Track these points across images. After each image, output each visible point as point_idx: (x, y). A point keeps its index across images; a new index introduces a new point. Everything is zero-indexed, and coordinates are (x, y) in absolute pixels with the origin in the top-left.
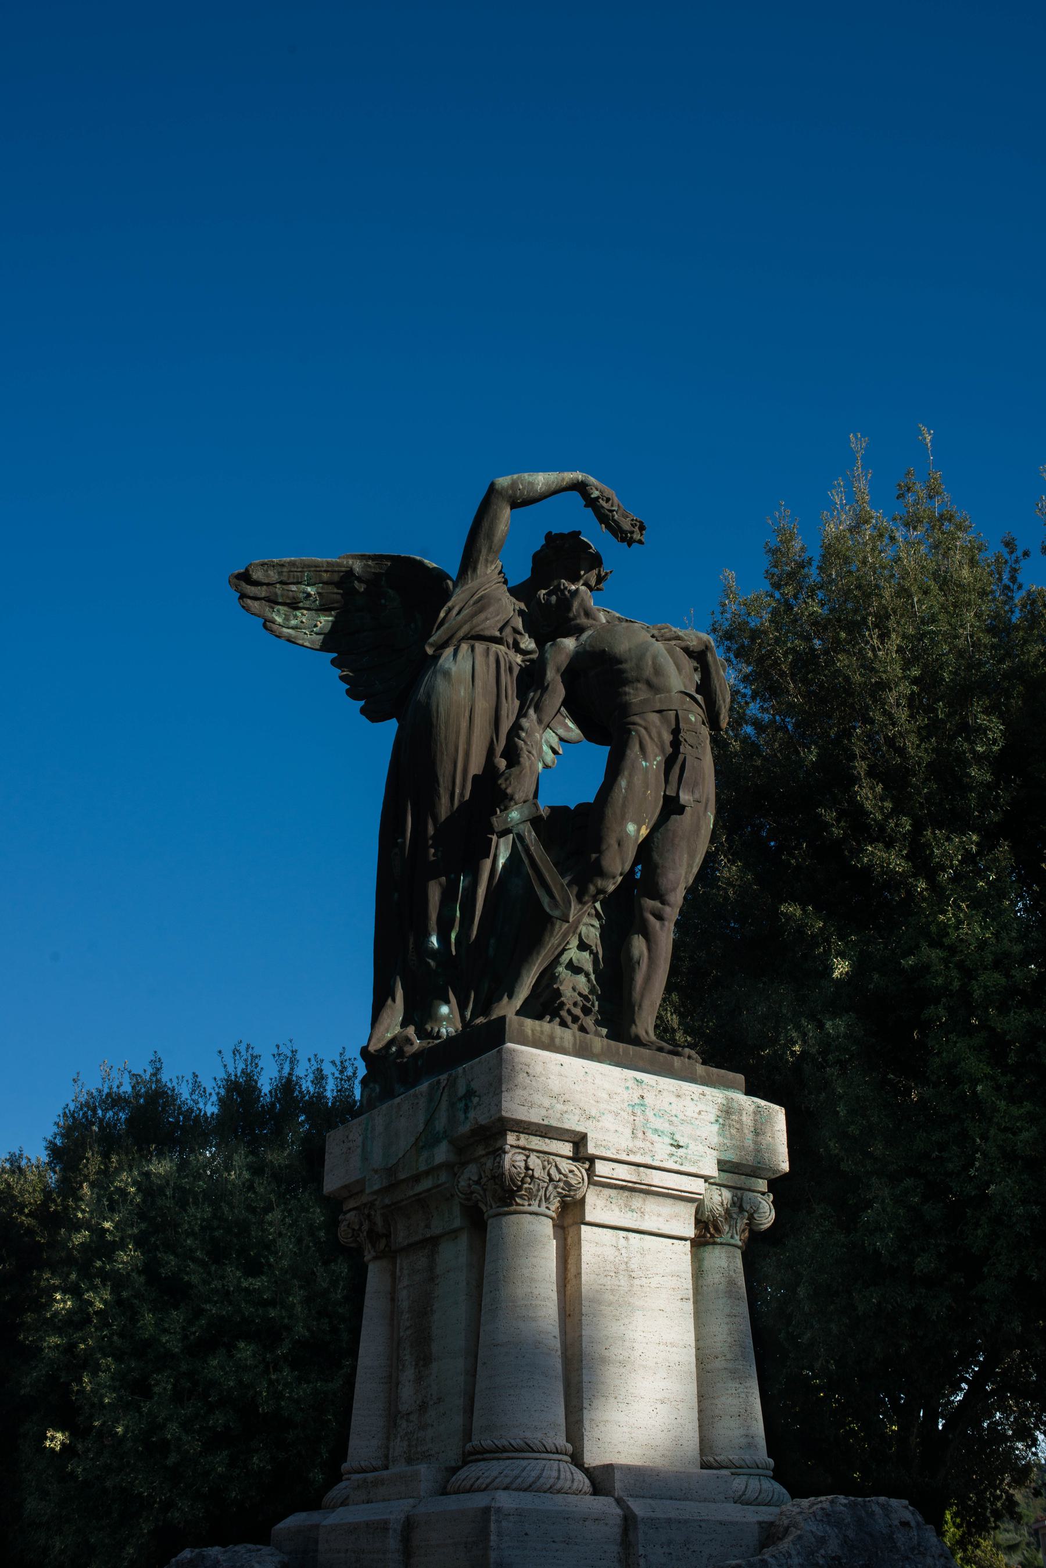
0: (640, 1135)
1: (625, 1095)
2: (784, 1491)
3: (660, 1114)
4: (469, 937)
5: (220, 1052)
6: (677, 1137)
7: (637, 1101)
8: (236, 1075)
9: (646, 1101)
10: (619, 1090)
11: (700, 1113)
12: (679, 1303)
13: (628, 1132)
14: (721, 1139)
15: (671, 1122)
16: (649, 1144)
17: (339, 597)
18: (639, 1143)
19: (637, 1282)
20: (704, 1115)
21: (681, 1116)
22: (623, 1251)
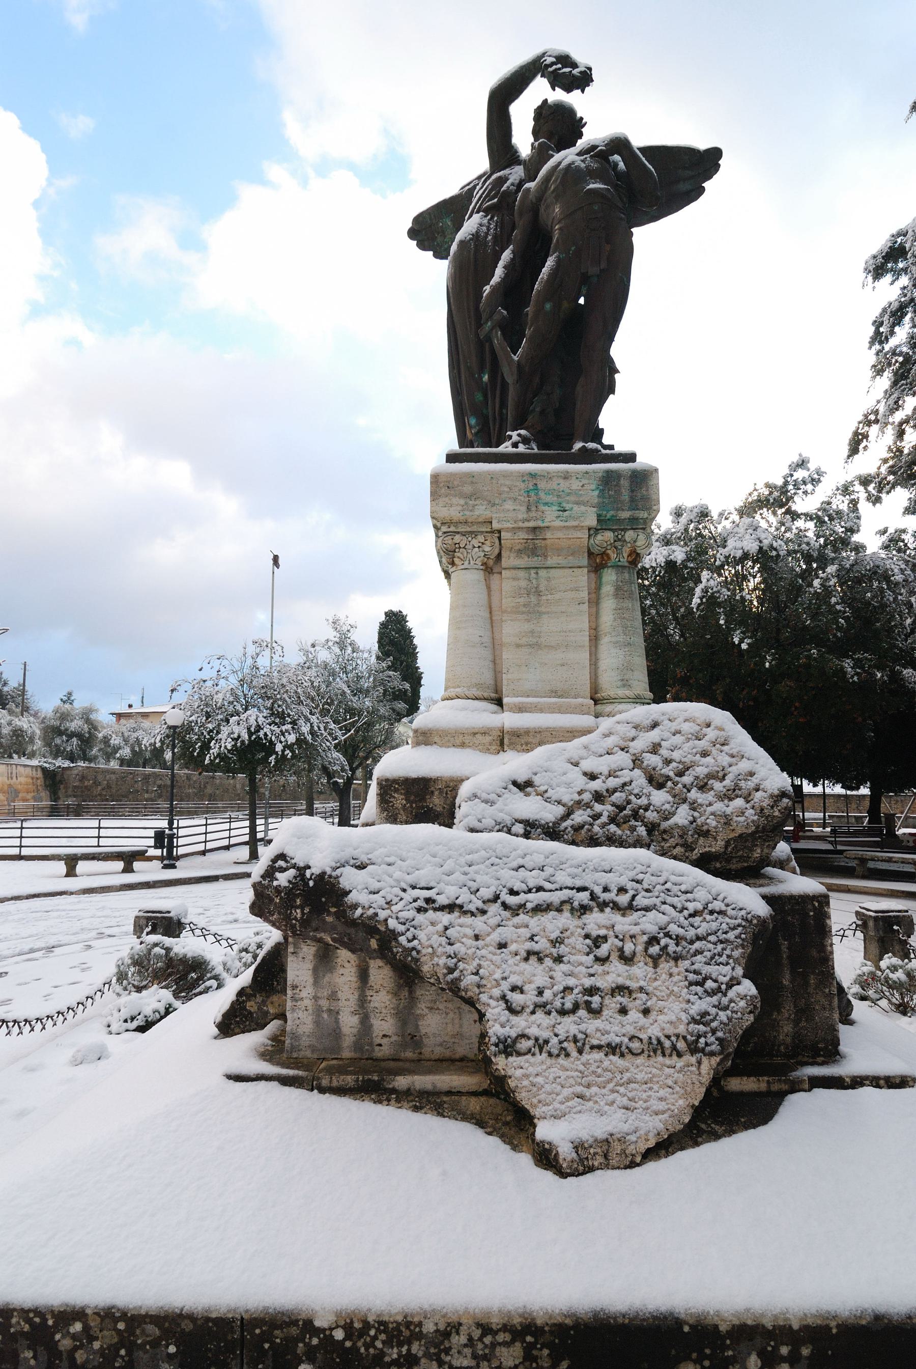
0: (534, 509)
1: (522, 485)
2: (700, 710)
3: (549, 492)
4: (559, 262)
5: (201, 670)
6: (564, 505)
7: (532, 487)
8: (431, 219)
9: (539, 486)
10: (518, 484)
11: (583, 486)
12: (577, 606)
13: (524, 509)
14: (601, 500)
15: (559, 496)
16: (540, 513)
17: (182, 832)
18: (533, 514)
19: (544, 598)
20: (586, 487)
21: (567, 491)
22: (534, 581)
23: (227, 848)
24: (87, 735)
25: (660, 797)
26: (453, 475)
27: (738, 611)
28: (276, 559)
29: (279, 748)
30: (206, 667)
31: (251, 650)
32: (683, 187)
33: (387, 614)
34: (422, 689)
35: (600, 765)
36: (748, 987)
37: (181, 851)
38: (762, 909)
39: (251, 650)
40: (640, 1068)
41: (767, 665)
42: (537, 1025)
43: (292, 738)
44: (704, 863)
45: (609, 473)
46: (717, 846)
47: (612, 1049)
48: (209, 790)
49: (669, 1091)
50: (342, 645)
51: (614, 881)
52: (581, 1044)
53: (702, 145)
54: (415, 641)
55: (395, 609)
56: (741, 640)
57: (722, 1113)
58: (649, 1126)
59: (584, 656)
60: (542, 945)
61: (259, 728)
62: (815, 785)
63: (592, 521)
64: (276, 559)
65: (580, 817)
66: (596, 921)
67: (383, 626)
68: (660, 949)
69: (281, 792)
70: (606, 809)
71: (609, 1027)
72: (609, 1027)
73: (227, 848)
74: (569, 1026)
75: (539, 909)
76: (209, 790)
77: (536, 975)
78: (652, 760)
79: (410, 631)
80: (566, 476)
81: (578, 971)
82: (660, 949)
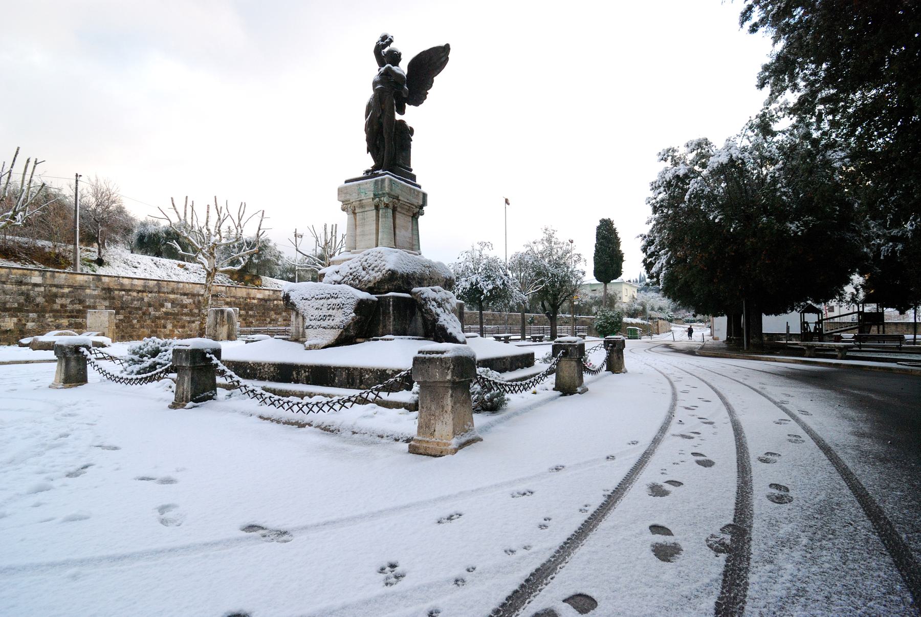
24: (501, 287)
25: (364, 273)
26: (350, 186)
27: (711, 198)
28: (507, 201)
29: (485, 292)
31: (478, 247)
32: (443, 59)
34: (623, 264)
35: (352, 266)
36: (354, 315)
39: (478, 247)
40: (327, 331)
42: (312, 323)
43: (490, 287)
46: (371, 285)
48: (510, 322)
51: (335, 292)
53: (443, 44)
54: (619, 236)
55: (606, 218)
56: (715, 217)
58: (325, 342)
59: (374, 237)
61: (477, 283)
62: (902, 312)
63: (372, 196)
64: (507, 201)
65: (346, 279)
66: (329, 301)
67: (599, 228)
68: (340, 307)
70: (351, 277)
71: (324, 324)
72: (324, 324)
74: (319, 323)
76: (510, 322)
77: (317, 313)
78: (365, 263)
79: (615, 230)
81: (325, 312)
82: (340, 307)
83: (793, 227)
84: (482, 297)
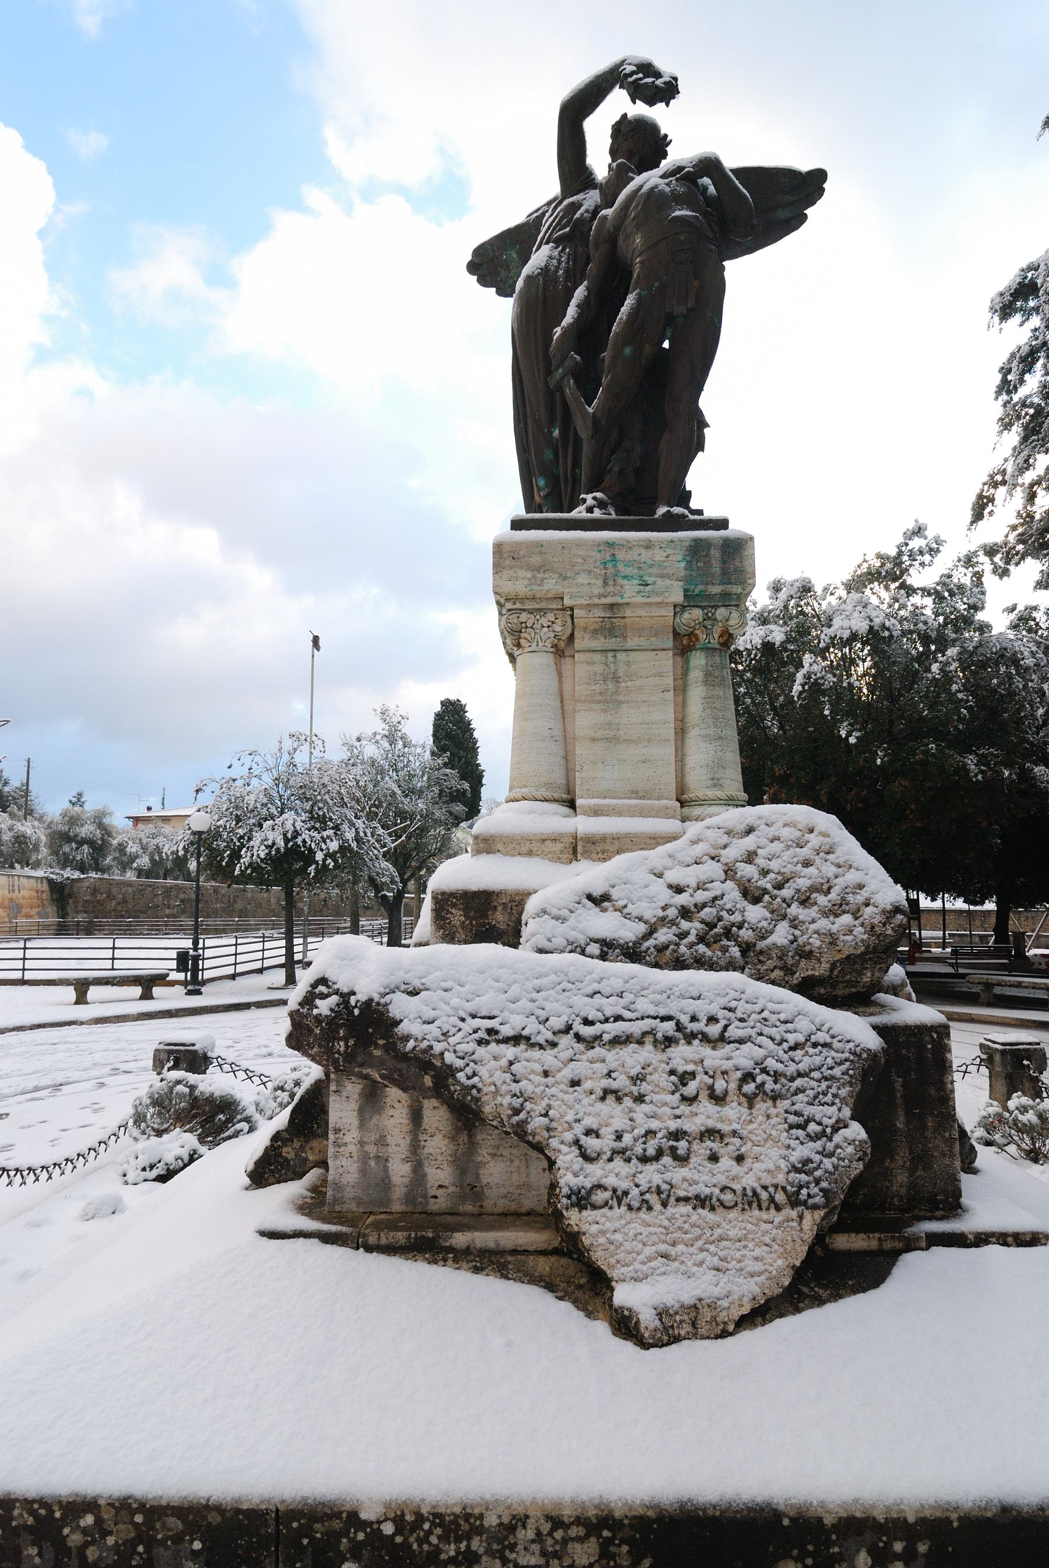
23: (260, 971)
24: (100, 842)
25: (755, 913)
26: (518, 544)
27: (845, 699)
28: (316, 641)
29: (319, 856)
30: (236, 764)
31: (288, 744)
32: (782, 214)
33: (443, 703)
35: (688, 876)
36: (856, 1131)
37: (207, 974)
38: (873, 1041)
39: (288, 744)
40: (733, 1223)
41: (879, 761)
42: (615, 1174)
43: (334, 846)
44: (807, 988)
45: (697, 541)
46: (821, 969)
47: (701, 1202)
48: (239, 905)
49: (766, 1249)
50: (391, 738)
51: (703, 1009)
52: (665, 1196)
53: (804, 166)
54: (476, 735)
55: (453, 698)
57: (827, 1274)
58: (744, 1290)
59: (670, 751)
60: (621, 1082)
61: (296, 834)
62: (933, 900)
63: (678, 597)
64: (316, 641)
65: (664, 935)
66: (682, 1055)
67: (439, 717)
68: (755, 1087)
69: (322, 907)
70: (694, 927)
71: (698, 1176)
72: (698, 1176)
73: (260, 971)
74: (651, 1175)
75: (618, 1041)
76: (239, 905)
77: (614, 1116)
78: (747, 871)
79: (469, 723)
80: (649, 545)
81: (661, 1112)
82: (755, 1087)
83: (1007, 773)
84: (312, 869)
